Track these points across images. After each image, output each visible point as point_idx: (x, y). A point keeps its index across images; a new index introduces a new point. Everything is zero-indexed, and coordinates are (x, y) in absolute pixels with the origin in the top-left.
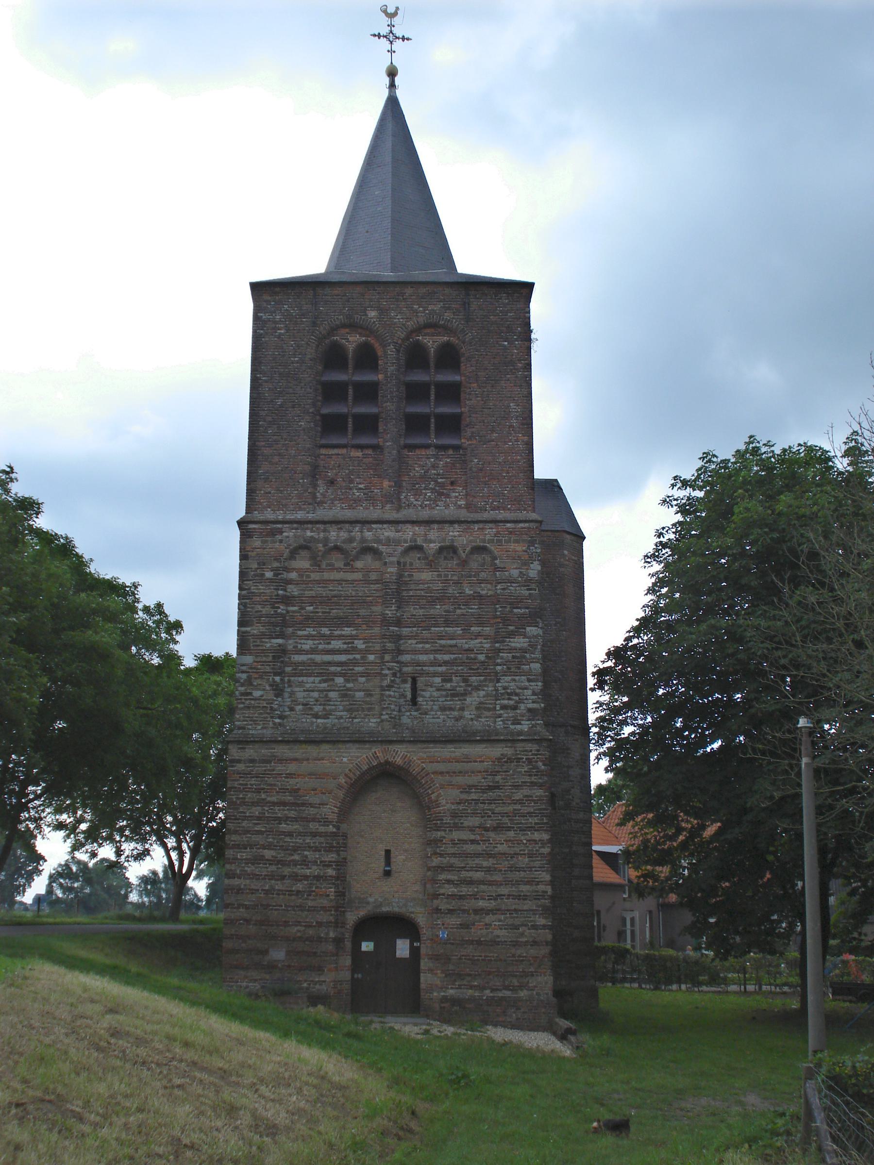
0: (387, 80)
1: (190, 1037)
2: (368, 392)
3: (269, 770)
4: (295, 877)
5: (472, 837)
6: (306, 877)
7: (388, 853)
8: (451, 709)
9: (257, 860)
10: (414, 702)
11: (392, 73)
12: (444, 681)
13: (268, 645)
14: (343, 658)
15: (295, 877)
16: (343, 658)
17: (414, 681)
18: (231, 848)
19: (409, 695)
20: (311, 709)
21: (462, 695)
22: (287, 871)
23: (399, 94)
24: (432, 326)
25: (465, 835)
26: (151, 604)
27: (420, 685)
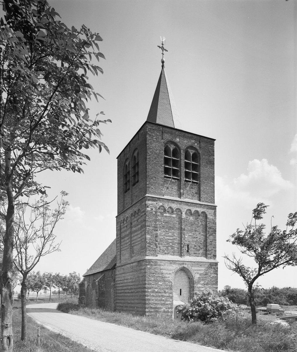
0: (161, 64)
1: (286, 306)
2: (175, 163)
3: (156, 268)
4: (162, 296)
5: (202, 286)
6: (165, 296)
7: (181, 289)
8: (196, 254)
9: (153, 292)
10: (188, 251)
11: (163, 62)
12: (195, 246)
13: (154, 233)
14: (172, 238)
15: (162, 296)
16: (172, 238)
17: (188, 245)
18: (146, 289)
19: (187, 250)
20: (164, 252)
21: (198, 250)
22: (160, 294)
23: (162, 69)
24: (192, 147)
25: (201, 286)
26: (287, 219)
27: (189, 247)
